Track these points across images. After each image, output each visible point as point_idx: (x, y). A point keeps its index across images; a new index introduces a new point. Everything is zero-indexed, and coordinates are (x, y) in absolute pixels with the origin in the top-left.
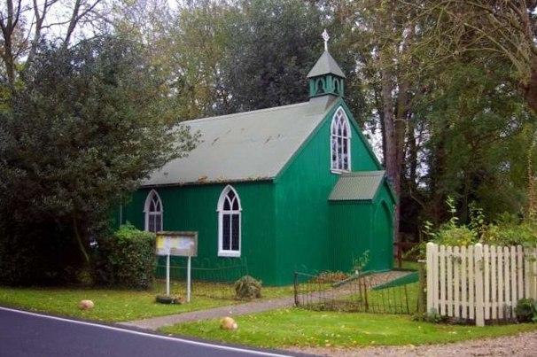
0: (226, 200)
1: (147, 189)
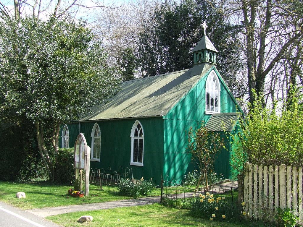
0: (136, 129)
1: (94, 122)
